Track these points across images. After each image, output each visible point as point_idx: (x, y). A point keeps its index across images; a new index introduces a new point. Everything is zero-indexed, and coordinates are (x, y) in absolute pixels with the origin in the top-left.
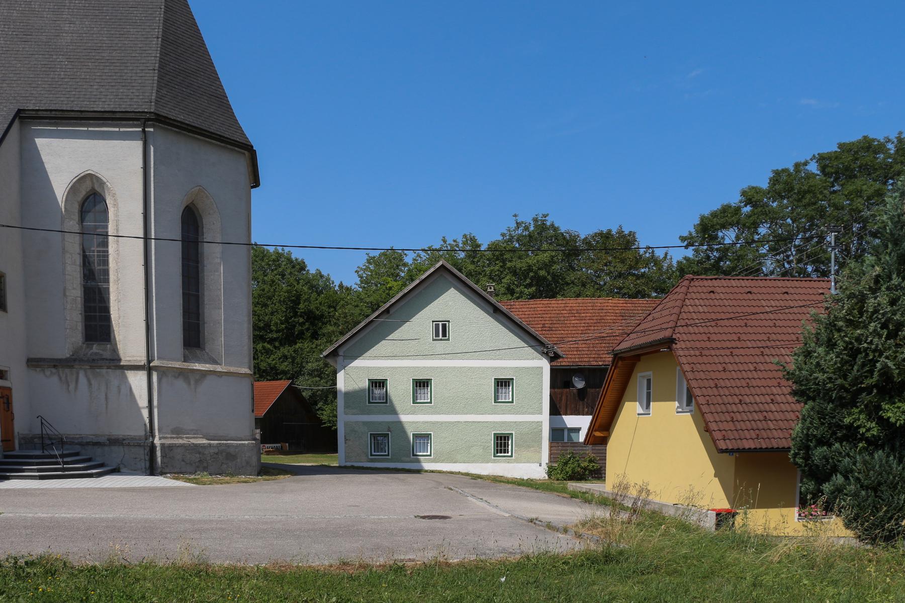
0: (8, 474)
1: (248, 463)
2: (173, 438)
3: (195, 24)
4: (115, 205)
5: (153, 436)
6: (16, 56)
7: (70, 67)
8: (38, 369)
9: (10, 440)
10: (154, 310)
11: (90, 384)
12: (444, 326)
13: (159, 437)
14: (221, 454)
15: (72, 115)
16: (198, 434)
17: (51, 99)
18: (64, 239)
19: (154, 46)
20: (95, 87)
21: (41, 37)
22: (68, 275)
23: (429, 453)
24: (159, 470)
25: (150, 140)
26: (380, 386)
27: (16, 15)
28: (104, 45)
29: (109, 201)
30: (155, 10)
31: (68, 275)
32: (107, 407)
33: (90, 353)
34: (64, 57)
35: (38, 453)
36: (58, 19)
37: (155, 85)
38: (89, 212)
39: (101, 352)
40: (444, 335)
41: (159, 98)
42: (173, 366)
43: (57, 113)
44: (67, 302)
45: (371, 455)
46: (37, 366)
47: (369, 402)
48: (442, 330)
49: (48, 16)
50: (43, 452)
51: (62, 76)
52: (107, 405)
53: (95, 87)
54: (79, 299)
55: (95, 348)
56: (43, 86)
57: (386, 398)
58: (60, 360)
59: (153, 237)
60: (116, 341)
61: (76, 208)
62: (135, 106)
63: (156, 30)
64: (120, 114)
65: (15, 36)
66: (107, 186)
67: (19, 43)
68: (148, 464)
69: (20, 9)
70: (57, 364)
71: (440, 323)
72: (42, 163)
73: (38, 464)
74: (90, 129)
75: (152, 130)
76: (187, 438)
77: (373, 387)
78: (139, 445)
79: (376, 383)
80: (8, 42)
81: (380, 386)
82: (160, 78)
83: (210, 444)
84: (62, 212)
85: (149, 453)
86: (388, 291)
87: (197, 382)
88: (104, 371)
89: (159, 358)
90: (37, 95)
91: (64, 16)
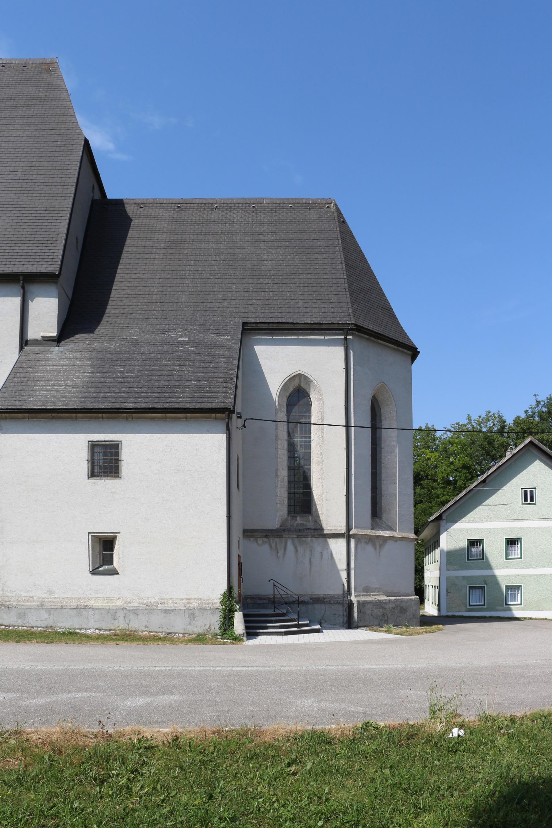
0: (258, 631)
1: (414, 615)
3: (361, 251)
5: (350, 595)
6: (230, 280)
7: (276, 287)
8: (252, 539)
10: (353, 486)
11: (296, 551)
13: (355, 595)
14: (397, 608)
15: (286, 326)
16: (380, 592)
17: (267, 314)
18: (277, 428)
19: (340, 270)
20: (300, 303)
21: (246, 264)
22: (279, 458)
23: (519, 602)
24: (355, 624)
25: (350, 346)
28: (299, 270)
29: (313, 396)
30: (334, 241)
31: (279, 458)
32: (310, 570)
36: (257, 250)
37: (349, 301)
38: (295, 405)
39: (305, 523)
41: (355, 311)
43: (274, 325)
44: (278, 481)
45: (470, 605)
46: (251, 536)
47: (468, 559)
49: (249, 248)
50: (274, 611)
51: (271, 295)
52: (310, 568)
54: (286, 478)
55: (299, 520)
56: (258, 303)
57: (482, 556)
58: (272, 531)
59: (353, 425)
60: (318, 513)
62: (338, 319)
63: (339, 257)
64: (326, 325)
67: (230, 270)
68: (345, 619)
69: (225, 243)
70: (268, 534)
71: (528, 490)
72: (260, 366)
74: (300, 337)
75: (351, 337)
76: (373, 595)
77: (471, 546)
78: (339, 603)
79: (474, 542)
80: (222, 269)
83: (389, 600)
84: (276, 405)
85: (347, 610)
86: (426, 462)
87: (381, 546)
88: (309, 539)
89: (356, 527)
91: (261, 247)
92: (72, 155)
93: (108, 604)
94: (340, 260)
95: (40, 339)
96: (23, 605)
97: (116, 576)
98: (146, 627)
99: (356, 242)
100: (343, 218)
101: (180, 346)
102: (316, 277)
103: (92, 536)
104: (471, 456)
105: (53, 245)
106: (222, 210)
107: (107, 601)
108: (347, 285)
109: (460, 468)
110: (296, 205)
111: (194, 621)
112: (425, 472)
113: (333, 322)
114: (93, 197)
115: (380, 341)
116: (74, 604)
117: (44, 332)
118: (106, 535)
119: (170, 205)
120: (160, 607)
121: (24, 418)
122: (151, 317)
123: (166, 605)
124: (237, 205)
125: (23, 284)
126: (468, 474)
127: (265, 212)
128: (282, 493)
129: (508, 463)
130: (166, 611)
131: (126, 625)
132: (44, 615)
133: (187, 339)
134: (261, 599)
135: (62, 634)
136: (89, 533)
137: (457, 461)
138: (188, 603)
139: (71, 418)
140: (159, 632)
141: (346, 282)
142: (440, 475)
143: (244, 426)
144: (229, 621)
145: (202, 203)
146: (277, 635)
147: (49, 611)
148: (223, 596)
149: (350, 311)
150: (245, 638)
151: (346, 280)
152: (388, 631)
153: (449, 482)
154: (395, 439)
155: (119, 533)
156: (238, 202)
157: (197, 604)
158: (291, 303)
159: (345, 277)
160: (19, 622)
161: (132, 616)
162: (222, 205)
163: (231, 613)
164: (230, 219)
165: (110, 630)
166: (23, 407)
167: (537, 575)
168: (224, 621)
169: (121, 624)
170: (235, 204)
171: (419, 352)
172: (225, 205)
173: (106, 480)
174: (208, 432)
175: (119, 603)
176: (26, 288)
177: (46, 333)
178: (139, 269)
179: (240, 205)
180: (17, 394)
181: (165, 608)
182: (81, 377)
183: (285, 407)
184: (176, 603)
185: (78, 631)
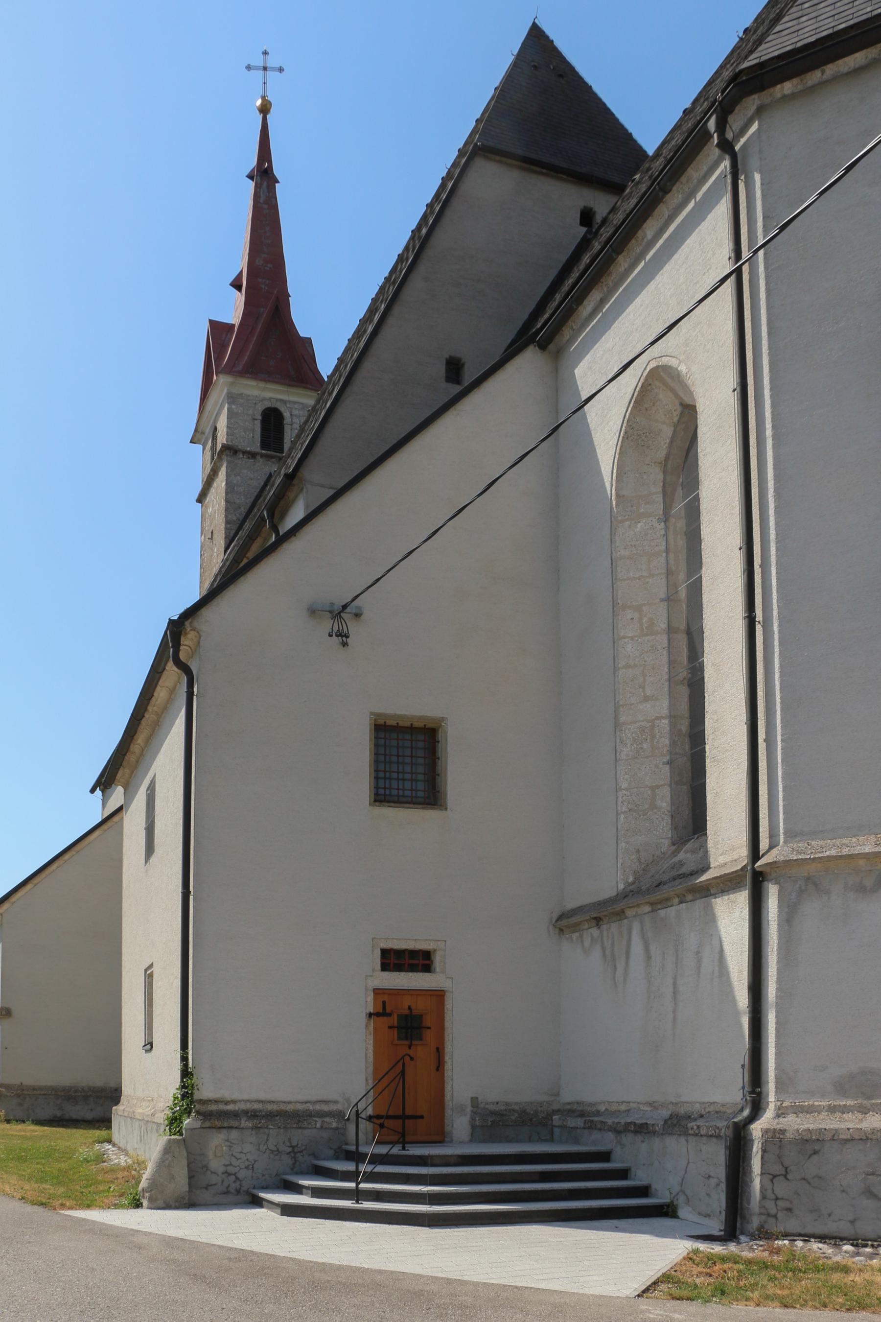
2: (844, 1110)
9: (422, 1117)
13: (779, 1108)
31: (628, 666)
32: (675, 1019)
42: (845, 851)
73: (378, 1196)
74: (648, 257)
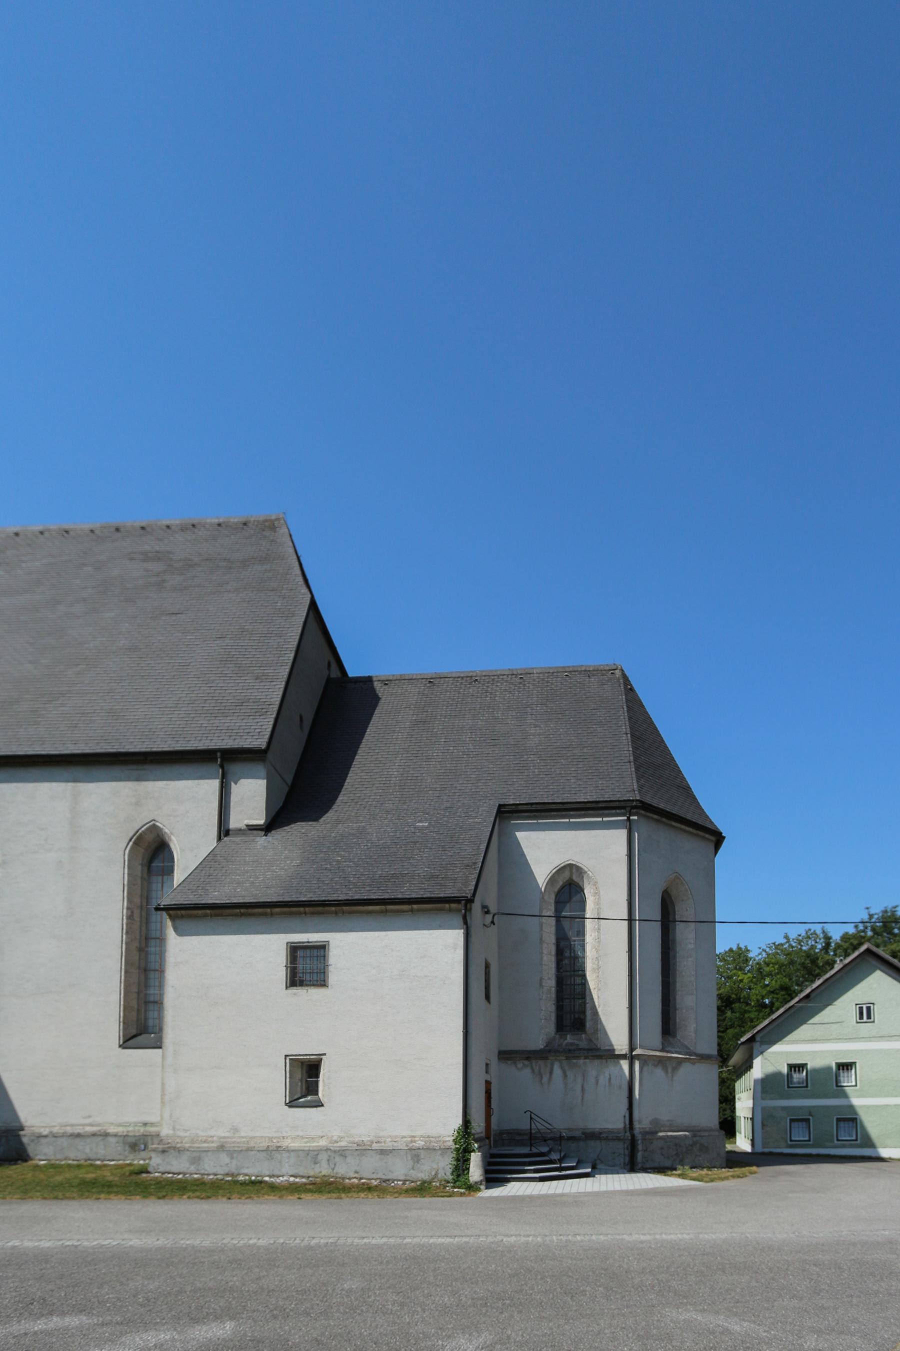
0: (509, 1176)
3: (652, 723)
4: (596, 893)
7: (543, 764)
8: (509, 1062)
11: (565, 1076)
12: (869, 1009)
15: (554, 807)
20: (572, 781)
22: (545, 965)
24: (640, 1166)
25: (634, 828)
26: (799, 1070)
27: (480, 723)
28: (573, 743)
31: (545, 965)
32: (583, 1099)
33: (564, 1044)
34: (535, 756)
35: (525, 1150)
39: (576, 1042)
40: (869, 1017)
41: (641, 787)
43: (538, 806)
46: (508, 1059)
47: (788, 1087)
48: (865, 1013)
49: (513, 722)
50: (531, 1150)
51: (537, 773)
53: (572, 781)
54: (553, 989)
55: (569, 1039)
56: (520, 783)
58: (534, 1052)
59: (637, 918)
61: (551, 899)
62: (618, 796)
65: (483, 741)
66: (589, 875)
68: (627, 1159)
70: (529, 1056)
73: (531, 1164)
74: (571, 820)
75: (636, 818)
78: (618, 1139)
81: (799, 1070)
82: (637, 769)
85: (629, 1147)
87: (675, 1069)
88: (581, 1061)
90: (514, 791)
92: (294, 618)
93: (308, 1145)
94: (624, 730)
95: (244, 827)
96: (199, 1147)
97: (319, 1109)
98: (356, 1172)
99: (647, 713)
100: (631, 685)
101: (418, 831)
102: (594, 751)
103: (290, 1059)
104: (789, 976)
105: (262, 717)
106: (483, 683)
107: (307, 1140)
108: (632, 758)
109: (778, 990)
110: (573, 673)
111: (419, 1165)
112: (736, 995)
113: (612, 799)
114: (329, 675)
115: (673, 823)
116: (264, 1144)
117: (249, 819)
118: (308, 1057)
119: (420, 681)
120: (375, 1146)
121: (205, 916)
122: (387, 802)
123: (383, 1144)
124: (501, 677)
125: (221, 762)
126: (786, 996)
127: (535, 682)
128: (548, 1007)
129: (838, 976)
130: (383, 1152)
131: (331, 1170)
132: (224, 1158)
133: (427, 824)
134: (520, 1134)
135: (241, 1184)
136: (286, 1056)
137: (774, 982)
138: (412, 1141)
139: (265, 914)
140: (372, 1179)
141: (631, 755)
142: (754, 998)
143: (493, 922)
144: (463, 1164)
145: (459, 677)
146: (530, 1181)
147: (231, 1154)
148: (458, 1132)
149: (635, 787)
150: (482, 1187)
151: (631, 752)
152: (682, 1176)
153: (764, 1006)
154: (693, 941)
155: (325, 1054)
156: (503, 673)
157: (423, 1143)
158: (561, 781)
159: (631, 749)
160: (192, 1169)
161: (338, 1159)
162: (483, 678)
163: (467, 1154)
164: (491, 693)
165: (309, 1177)
166: (203, 902)
167: (877, 1106)
168: (458, 1165)
169: (323, 1169)
170: (498, 676)
171: (724, 838)
172: (486, 678)
173: (309, 990)
174: (440, 927)
175: (323, 1143)
176: (226, 768)
177: (251, 821)
178: (377, 751)
179: (505, 677)
180: (200, 888)
181: (382, 1148)
182: (286, 867)
183: (553, 905)
184: (395, 1142)
185: (267, 1179)
